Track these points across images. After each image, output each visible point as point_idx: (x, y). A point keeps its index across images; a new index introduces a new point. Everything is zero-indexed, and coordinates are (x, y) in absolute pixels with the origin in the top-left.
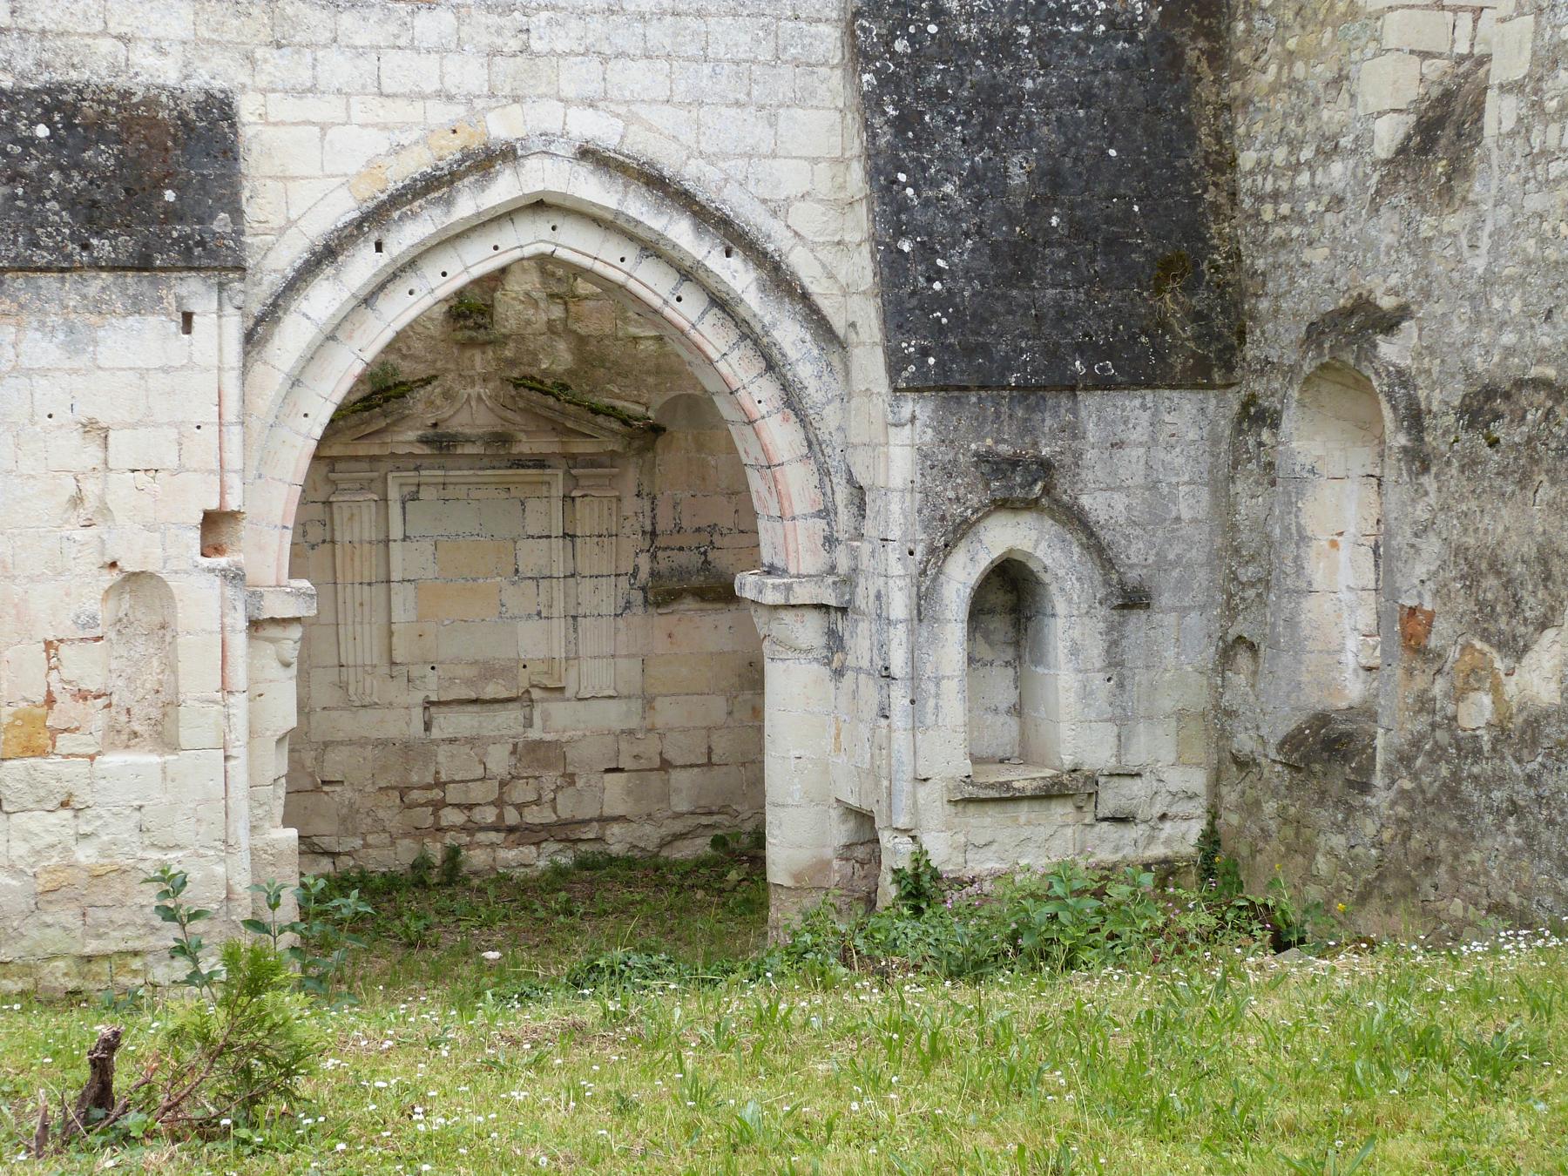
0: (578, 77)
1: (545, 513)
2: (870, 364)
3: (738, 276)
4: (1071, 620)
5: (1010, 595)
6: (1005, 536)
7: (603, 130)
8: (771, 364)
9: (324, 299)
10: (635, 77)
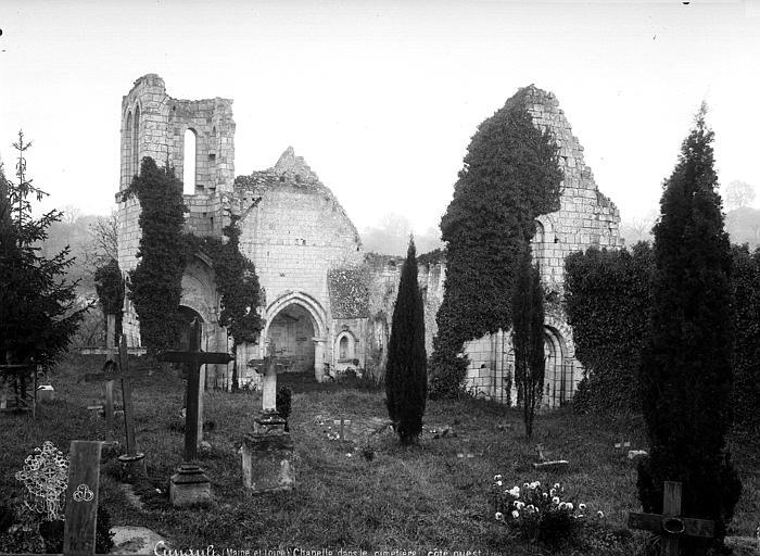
0: (299, 285)
1: (284, 329)
2: (330, 315)
3: (315, 305)
4: (351, 343)
5: (344, 339)
6: (344, 334)
7: (302, 290)
8: (314, 309)
9: (272, 309)
10: (306, 284)
